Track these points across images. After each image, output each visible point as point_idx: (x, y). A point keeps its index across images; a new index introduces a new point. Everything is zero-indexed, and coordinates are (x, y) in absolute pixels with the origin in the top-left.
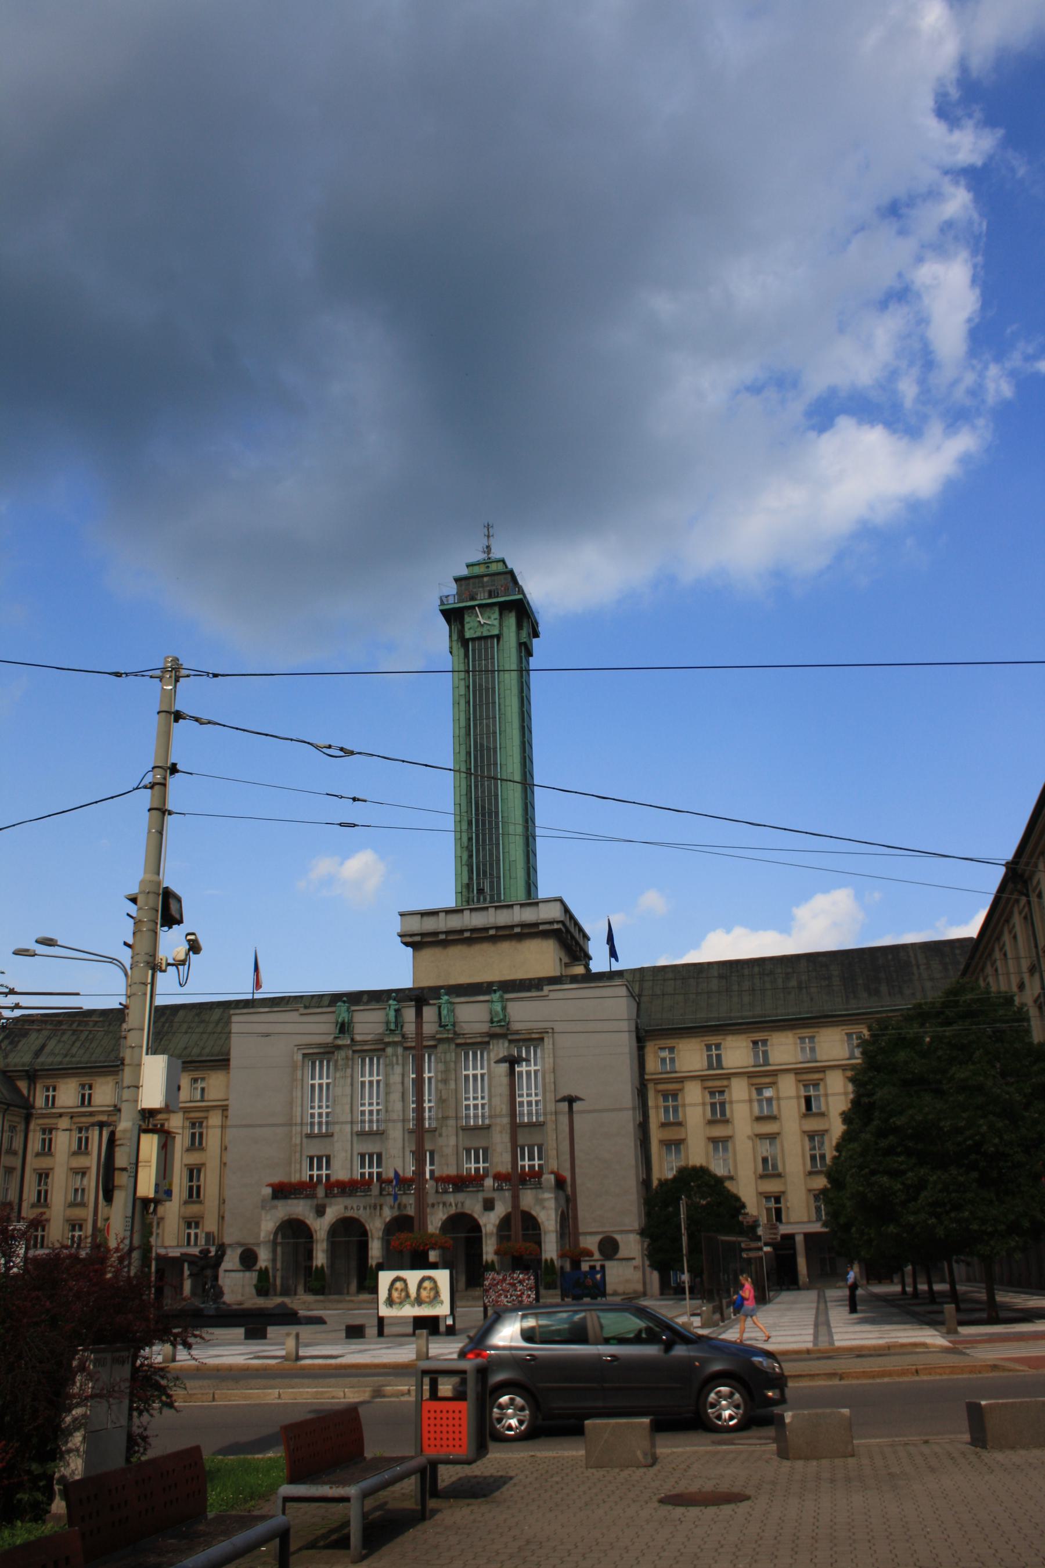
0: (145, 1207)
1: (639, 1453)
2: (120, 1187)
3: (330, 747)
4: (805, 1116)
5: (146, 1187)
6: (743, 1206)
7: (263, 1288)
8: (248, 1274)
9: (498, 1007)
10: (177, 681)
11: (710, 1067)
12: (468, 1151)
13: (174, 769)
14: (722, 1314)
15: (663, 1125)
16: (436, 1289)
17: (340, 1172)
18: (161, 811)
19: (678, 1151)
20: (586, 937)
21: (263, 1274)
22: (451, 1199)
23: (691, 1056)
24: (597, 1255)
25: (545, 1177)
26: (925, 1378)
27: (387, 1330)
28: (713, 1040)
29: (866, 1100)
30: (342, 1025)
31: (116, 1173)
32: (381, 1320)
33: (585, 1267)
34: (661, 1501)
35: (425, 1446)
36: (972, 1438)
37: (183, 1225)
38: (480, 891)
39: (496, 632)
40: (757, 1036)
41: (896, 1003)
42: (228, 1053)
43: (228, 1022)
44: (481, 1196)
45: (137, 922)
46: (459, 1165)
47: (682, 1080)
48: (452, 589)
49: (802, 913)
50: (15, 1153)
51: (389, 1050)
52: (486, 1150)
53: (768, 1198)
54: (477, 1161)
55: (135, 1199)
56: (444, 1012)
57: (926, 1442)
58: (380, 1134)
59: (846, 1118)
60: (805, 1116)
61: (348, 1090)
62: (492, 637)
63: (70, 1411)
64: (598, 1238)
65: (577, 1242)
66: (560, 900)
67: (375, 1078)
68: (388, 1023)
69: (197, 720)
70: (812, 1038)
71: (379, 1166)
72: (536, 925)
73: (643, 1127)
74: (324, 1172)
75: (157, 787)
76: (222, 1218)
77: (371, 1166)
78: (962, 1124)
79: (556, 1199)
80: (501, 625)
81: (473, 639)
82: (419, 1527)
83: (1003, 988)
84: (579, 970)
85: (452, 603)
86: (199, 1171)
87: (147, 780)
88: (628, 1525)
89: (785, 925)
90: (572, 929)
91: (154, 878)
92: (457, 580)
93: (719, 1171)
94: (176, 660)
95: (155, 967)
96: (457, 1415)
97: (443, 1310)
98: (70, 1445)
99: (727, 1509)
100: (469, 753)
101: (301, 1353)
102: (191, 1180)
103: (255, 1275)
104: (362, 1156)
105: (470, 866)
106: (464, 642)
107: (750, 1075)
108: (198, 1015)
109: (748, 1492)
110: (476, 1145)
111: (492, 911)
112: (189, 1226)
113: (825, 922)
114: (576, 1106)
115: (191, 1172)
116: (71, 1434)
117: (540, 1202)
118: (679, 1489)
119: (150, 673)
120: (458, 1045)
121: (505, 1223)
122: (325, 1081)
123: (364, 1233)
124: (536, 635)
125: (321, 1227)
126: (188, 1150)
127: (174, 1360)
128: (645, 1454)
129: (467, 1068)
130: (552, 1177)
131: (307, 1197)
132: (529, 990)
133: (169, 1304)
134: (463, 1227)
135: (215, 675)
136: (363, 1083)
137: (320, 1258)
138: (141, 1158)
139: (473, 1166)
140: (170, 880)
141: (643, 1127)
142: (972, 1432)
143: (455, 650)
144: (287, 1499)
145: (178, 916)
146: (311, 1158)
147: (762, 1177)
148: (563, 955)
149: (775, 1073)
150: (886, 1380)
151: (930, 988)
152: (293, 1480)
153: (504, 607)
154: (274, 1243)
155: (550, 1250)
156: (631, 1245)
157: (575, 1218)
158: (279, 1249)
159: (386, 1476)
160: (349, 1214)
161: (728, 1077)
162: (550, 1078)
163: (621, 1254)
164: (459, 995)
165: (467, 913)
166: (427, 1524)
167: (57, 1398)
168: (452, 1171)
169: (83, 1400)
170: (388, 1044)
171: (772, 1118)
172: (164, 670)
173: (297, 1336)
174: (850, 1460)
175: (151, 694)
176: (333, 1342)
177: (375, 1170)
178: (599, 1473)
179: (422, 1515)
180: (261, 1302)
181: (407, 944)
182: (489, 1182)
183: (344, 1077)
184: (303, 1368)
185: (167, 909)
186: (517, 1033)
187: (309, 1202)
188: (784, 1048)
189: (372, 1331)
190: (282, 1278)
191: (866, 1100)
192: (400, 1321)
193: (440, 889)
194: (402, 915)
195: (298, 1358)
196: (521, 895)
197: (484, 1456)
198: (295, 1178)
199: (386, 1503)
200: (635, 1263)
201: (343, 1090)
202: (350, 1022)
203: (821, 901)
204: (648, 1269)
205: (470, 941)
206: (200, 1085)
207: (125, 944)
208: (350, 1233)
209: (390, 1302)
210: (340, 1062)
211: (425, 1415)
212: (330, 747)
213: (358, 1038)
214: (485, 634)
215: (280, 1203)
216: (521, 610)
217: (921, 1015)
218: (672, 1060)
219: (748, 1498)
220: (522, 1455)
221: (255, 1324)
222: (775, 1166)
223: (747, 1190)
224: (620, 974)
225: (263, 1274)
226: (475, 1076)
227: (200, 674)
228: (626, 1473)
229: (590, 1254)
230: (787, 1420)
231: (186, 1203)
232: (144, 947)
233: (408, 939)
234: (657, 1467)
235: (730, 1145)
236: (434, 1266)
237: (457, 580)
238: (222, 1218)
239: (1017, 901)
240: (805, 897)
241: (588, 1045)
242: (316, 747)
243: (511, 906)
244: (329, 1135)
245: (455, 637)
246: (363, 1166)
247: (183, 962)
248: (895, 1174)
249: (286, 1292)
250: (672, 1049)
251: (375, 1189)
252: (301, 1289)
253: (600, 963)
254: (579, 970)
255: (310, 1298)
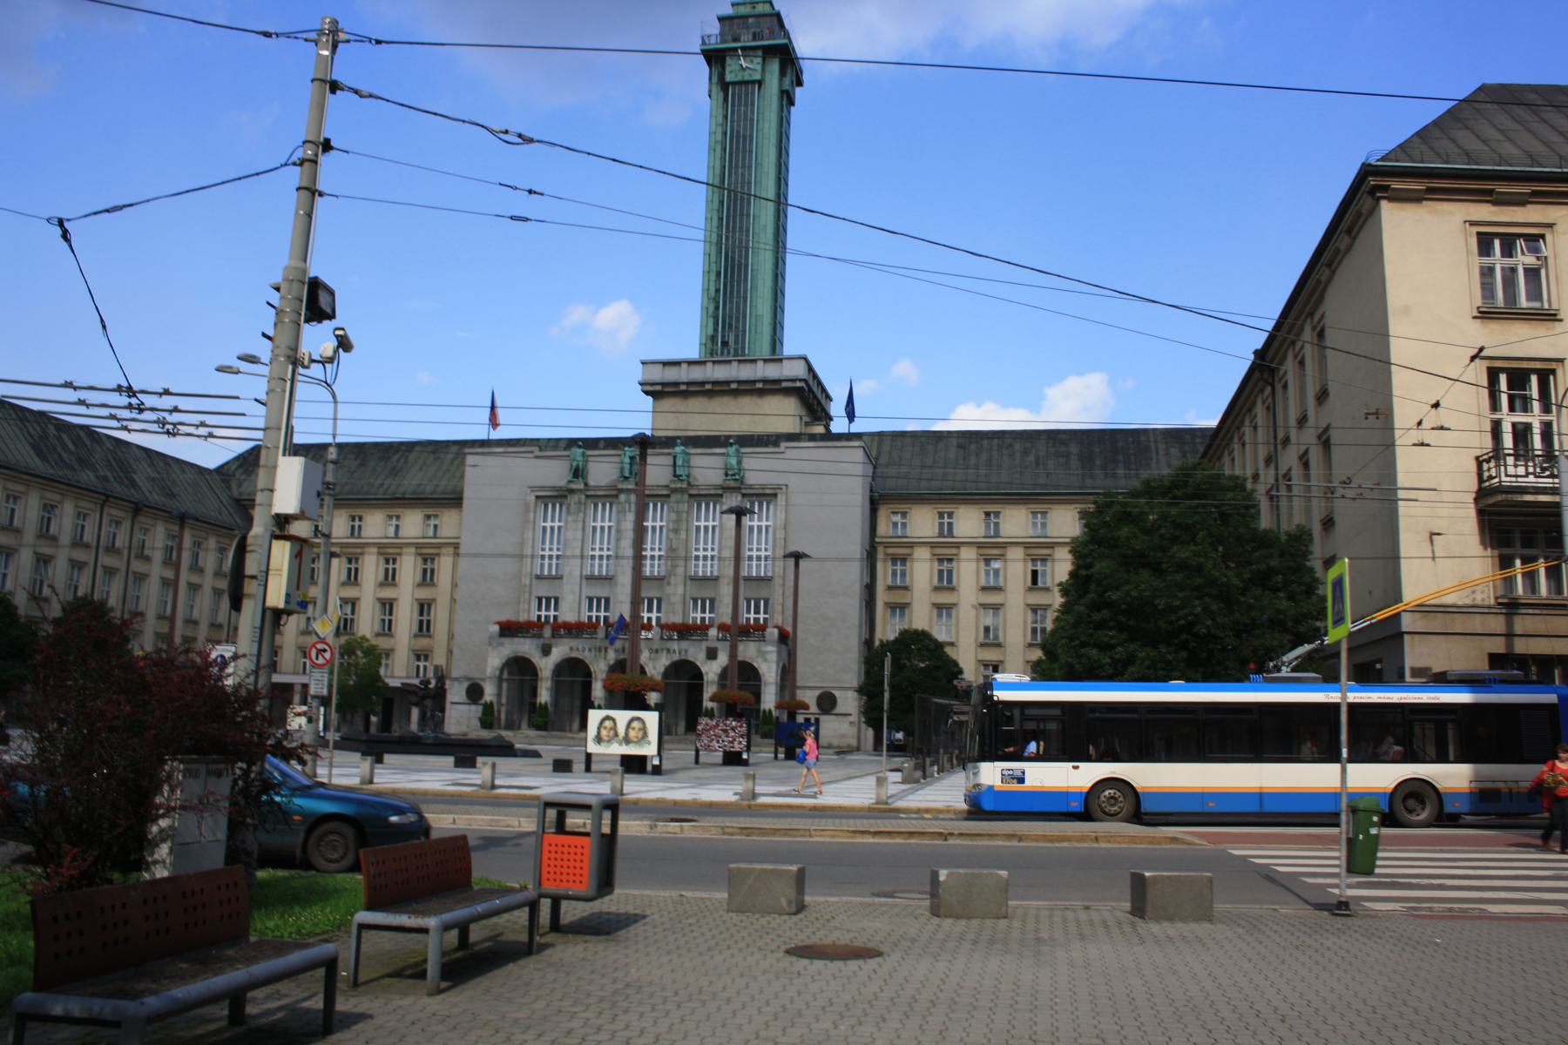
0: (275, 617)
1: (783, 901)
2: (249, 596)
3: (506, 132)
4: (1030, 589)
5: (276, 598)
6: (961, 672)
7: (488, 720)
8: (473, 707)
9: (733, 461)
10: (335, 47)
11: (941, 535)
12: (695, 601)
13: (327, 146)
14: (924, 771)
15: (890, 588)
16: (644, 730)
17: (568, 614)
18: (311, 192)
19: (902, 615)
20: (829, 398)
21: (488, 708)
22: (675, 646)
23: (923, 522)
24: (814, 708)
25: (769, 630)
26: (1104, 845)
27: (594, 767)
28: (947, 508)
29: (1084, 572)
30: (578, 471)
31: (246, 581)
32: (589, 756)
33: (800, 719)
34: (788, 952)
35: (544, 881)
36: (1132, 906)
37: (412, 657)
38: (725, 344)
39: (758, 77)
40: (990, 508)
41: (1124, 482)
42: (461, 492)
43: (463, 463)
44: (704, 645)
45: (279, 313)
46: (685, 613)
47: (911, 545)
48: (714, 28)
49: (1053, 393)
50: (118, 552)
51: (622, 497)
52: (712, 601)
53: (986, 666)
54: (703, 611)
55: (264, 609)
56: (679, 462)
57: (1087, 908)
58: (608, 579)
59: (1065, 590)
60: (1030, 589)
61: (579, 534)
62: (753, 82)
63: (155, 820)
64: (817, 693)
65: (793, 695)
66: (805, 359)
67: (607, 524)
68: (622, 469)
69: (356, 92)
70: (1044, 513)
71: (606, 610)
72: (778, 381)
73: (870, 589)
74: (552, 613)
75: (307, 165)
76: (450, 652)
77: (598, 610)
78: (1177, 603)
79: (779, 653)
80: (763, 69)
81: (734, 83)
82: (522, 962)
83: (1237, 472)
84: (820, 429)
85: (714, 43)
86: (429, 606)
87: (299, 154)
88: (742, 975)
89: (1035, 407)
90: (815, 389)
91: (300, 264)
92: (721, 19)
93: (940, 635)
94: (335, 22)
95: (296, 362)
96: (579, 850)
97: (650, 749)
98: (156, 856)
99: (853, 965)
100: (722, 202)
101: (497, 782)
102: (421, 614)
103: (480, 708)
104: (591, 600)
105: (716, 318)
106: (725, 86)
107: (980, 546)
108: (434, 452)
109: (883, 948)
110: (704, 595)
111: (735, 364)
112: (418, 659)
113: (1076, 403)
114: (802, 563)
115: (422, 606)
116: (157, 845)
117: (762, 654)
118: (814, 940)
119: (305, 35)
120: (691, 496)
121: (724, 675)
122: (557, 524)
123: (588, 674)
124: (800, 83)
125: (545, 666)
126: (419, 585)
127: (371, 782)
128: (790, 902)
129: (698, 519)
130: (776, 631)
131: (534, 636)
132: (766, 445)
133: (397, 731)
134: (685, 677)
135: (379, 42)
136: (594, 528)
137: (544, 696)
138: (272, 565)
139: (699, 615)
140: (317, 268)
141: (870, 589)
142: (1133, 901)
143: (714, 94)
144: (363, 927)
145: (329, 310)
146: (540, 600)
147: (983, 645)
148: (803, 413)
149: (1004, 546)
150: (1065, 844)
151: (1163, 468)
152: (371, 906)
153: (769, 52)
154: (500, 680)
155: (769, 700)
156: (849, 702)
157: (794, 671)
158: (505, 685)
159: (480, 908)
160: (574, 655)
161: (958, 545)
162: (780, 534)
163: (838, 710)
164: (696, 446)
165: (709, 365)
166: (534, 958)
167: (144, 810)
168: (678, 619)
169: (170, 810)
170: (621, 491)
171: (998, 589)
172: (321, 32)
173: (494, 765)
174: (1003, 922)
175: (306, 59)
176: (539, 775)
177: (602, 614)
178: (736, 918)
179: (528, 949)
180: (486, 734)
181: (647, 393)
182: (713, 632)
183: (576, 521)
184: (497, 797)
185: (315, 302)
186: (751, 487)
187: (535, 641)
188: (1016, 522)
189: (579, 766)
190: (508, 713)
191: (1084, 572)
192: (605, 758)
193: (684, 339)
194: (643, 363)
195: (493, 787)
196: (765, 351)
197: (611, 892)
198: (523, 618)
199: (501, 934)
200: (852, 719)
201: (574, 534)
202: (585, 466)
203: (1073, 383)
204: (863, 726)
205: (710, 394)
206: (433, 522)
207: (264, 335)
208: (574, 674)
209: (599, 739)
210: (573, 506)
211: (546, 847)
212: (506, 132)
213: (592, 483)
214: (747, 78)
215: (506, 641)
216: (785, 57)
217: (1149, 490)
218: (904, 525)
219: (879, 954)
220: (667, 894)
221: (465, 753)
222: (996, 637)
223: (967, 658)
224: (858, 436)
225: (488, 708)
226: (706, 528)
227: (362, 39)
228: (763, 921)
229: (806, 707)
230: (942, 878)
231: (416, 636)
232: (284, 340)
233: (649, 388)
234: (801, 916)
235: (954, 612)
236: (646, 707)
237: (721, 19)
238: (450, 652)
239: (1262, 391)
240: (1058, 376)
241: (820, 500)
242: (491, 131)
243: (754, 361)
244: (559, 578)
245: (715, 80)
246: (590, 609)
247: (331, 360)
248: (1105, 647)
249: (510, 726)
250: (904, 515)
251: (601, 633)
252: (524, 724)
253: (839, 425)
254: (820, 429)
255: (533, 733)
